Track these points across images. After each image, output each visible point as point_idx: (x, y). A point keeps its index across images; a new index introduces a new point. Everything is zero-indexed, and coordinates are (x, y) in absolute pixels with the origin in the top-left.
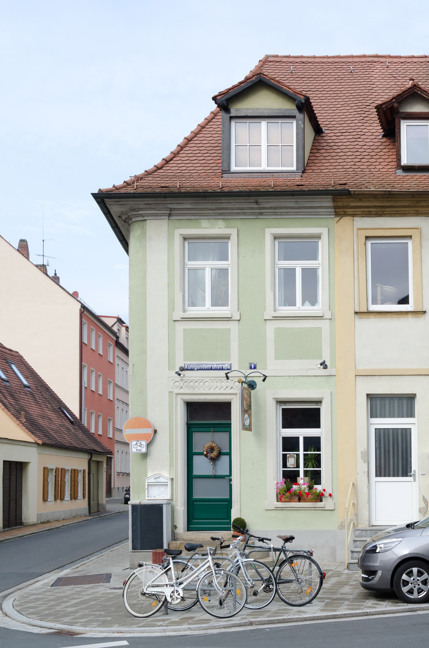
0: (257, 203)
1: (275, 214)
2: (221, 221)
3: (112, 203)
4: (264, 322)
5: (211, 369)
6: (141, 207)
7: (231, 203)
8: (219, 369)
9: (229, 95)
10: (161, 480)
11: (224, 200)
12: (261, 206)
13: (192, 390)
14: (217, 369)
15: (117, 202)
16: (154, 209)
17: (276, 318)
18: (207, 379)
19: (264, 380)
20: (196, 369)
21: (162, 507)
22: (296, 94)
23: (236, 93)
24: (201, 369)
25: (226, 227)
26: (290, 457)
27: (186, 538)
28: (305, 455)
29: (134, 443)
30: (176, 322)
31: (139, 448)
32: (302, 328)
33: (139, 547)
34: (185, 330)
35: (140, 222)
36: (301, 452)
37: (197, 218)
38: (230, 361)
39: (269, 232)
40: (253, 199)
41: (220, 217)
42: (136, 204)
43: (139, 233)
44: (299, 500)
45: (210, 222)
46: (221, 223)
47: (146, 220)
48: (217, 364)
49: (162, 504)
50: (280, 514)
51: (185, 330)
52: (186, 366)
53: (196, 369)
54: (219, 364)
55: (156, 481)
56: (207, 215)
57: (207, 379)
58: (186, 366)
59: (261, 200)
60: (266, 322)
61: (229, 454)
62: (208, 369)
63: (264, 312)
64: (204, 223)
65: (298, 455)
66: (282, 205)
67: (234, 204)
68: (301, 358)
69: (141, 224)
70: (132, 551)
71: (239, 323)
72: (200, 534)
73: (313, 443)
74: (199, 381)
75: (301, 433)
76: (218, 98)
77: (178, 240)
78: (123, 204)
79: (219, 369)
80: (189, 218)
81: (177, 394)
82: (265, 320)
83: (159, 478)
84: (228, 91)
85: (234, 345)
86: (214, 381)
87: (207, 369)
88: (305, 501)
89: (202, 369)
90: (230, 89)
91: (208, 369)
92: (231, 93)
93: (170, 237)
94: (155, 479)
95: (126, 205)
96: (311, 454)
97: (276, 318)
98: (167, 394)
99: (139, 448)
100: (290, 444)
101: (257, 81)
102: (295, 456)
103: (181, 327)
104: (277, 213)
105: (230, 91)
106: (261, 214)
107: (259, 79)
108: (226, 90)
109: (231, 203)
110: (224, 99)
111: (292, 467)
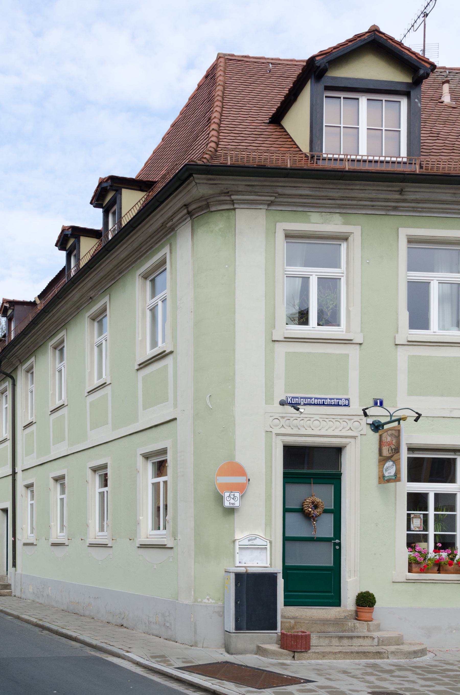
0: (401, 192)
1: (414, 210)
2: (337, 215)
3: (201, 182)
4: (394, 347)
5: (324, 404)
6: (240, 189)
7: (365, 190)
8: (334, 405)
9: (332, 55)
10: (258, 542)
11: (358, 185)
12: (405, 197)
13: (297, 429)
14: (331, 405)
15: (210, 179)
16: (256, 193)
17: (412, 343)
18: (317, 417)
19: (416, 420)
20: (302, 403)
21: (276, 577)
22: (420, 61)
23: (342, 53)
24: (309, 404)
25: (345, 224)
26: (415, 518)
27: (289, 615)
28: (436, 517)
29: (227, 494)
30: (276, 342)
31: (232, 501)
32: (445, 357)
33: (245, 627)
34: (287, 354)
35: (223, 212)
36: (431, 512)
37: (307, 209)
38: (347, 394)
39: (405, 232)
40: (397, 186)
41: (338, 211)
42: (233, 185)
43: (221, 226)
44: (439, 571)
45: (322, 216)
46: (337, 218)
47: (234, 209)
48: (331, 399)
49: (276, 573)
50: (411, 587)
51: (287, 354)
52: (289, 400)
53: (302, 403)
54: (334, 399)
55: (250, 543)
56: (320, 207)
57: (317, 417)
58: (289, 400)
59: (409, 187)
60: (397, 348)
61: (286, 510)
62: (319, 404)
63: (396, 335)
64: (315, 217)
65: (426, 516)
66: (434, 196)
67: (370, 191)
68: (442, 395)
69: (225, 214)
70: (234, 631)
71: (360, 347)
72: (307, 610)
73: (446, 502)
74: (306, 419)
75: (431, 489)
76: (317, 58)
77: (280, 236)
78: (216, 184)
79: (334, 405)
80: (294, 209)
81: (277, 435)
82: (396, 345)
83: (254, 539)
84: (332, 50)
85: (354, 375)
86: (325, 420)
87: (317, 404)
88: (447, 572)
89: (311, 404)
90: (335, 48)
91: (319, 404)
92: (334, 54)
93: (271, 233)
94: (249, 540)
95: (220, 186)
96: (442, 514)
97: (412, 343)
98: (264, 434)
99: (232, 501)
100: (417, 502)
101: (370, 39)
102: (422, 516)
103: (282, 350)
104: (418, 209)
105: (334, 51)
106: (395, 208)
107: (373, 38)
108: (329, 48)
109: (365, 190)
110: (325, 61)
111: (418, 529)
